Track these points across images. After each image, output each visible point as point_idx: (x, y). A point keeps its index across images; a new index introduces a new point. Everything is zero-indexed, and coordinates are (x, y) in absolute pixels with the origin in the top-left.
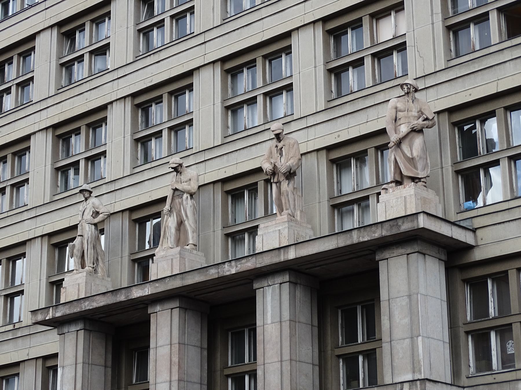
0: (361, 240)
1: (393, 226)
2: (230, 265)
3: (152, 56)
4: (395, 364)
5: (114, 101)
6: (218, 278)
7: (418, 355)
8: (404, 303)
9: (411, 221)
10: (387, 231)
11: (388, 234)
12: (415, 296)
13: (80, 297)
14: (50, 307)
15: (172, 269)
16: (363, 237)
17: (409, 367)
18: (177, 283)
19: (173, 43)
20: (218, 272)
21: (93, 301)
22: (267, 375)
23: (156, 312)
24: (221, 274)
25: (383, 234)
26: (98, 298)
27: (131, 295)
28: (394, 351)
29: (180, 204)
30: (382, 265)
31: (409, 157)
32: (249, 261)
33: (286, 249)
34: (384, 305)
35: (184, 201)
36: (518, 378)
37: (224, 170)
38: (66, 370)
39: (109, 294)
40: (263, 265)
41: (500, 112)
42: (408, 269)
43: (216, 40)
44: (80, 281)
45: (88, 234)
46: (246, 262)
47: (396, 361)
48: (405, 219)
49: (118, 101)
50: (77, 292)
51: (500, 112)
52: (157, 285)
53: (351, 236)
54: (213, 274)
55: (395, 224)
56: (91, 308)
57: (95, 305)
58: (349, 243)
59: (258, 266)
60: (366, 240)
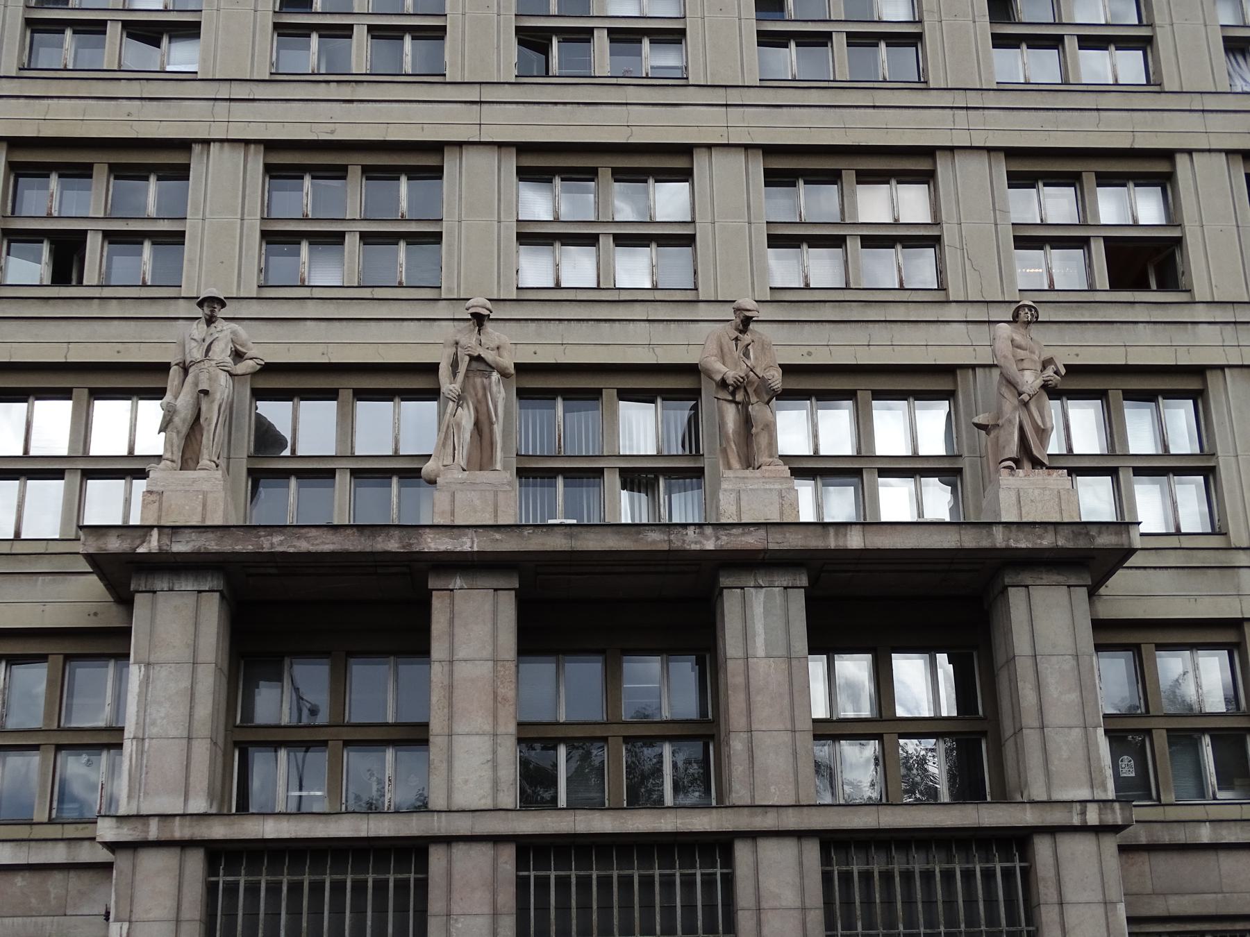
0: (1013, 544)
1: (1080, 534)
2: (702, 534)
3: (332, 85)
4: (1053, 768)
5: (215, 140)
6: (669, 551)
7: (1099, 759)
8: (1067, 667)
9: (1116, 534)
10: (1067, 539)
11: (1070, 545)
12: (1087, 658)
13: (208, 523)
14: (152, 527)
15: (496, 511)
16: (1016, 541)
17: (1084, 776)
18: (211, 544)
19: (312, 79)
20: (670, 541)
21: (299, 538)
22: (757, 753)
23: (452, 590)
24: (677, 545)
25: (1060, 543)
26: (314, 532)
27: (419, 544)
28: (1051, 747)
29: (484, 388)
30: (439, 604)
31: (1038, 427)
32: (750, 533)
33: (842, 529)
34: (1023, 667)
35: (493, 384)
36: (1245, 817)
37: (533, 348)
38: (161, 674)
39: (349, 531)
40: (785, 546)
41: (346, 395)
42: (196, 625)
43: (508, 106)
44: (206, 487)
45: (223, 393)
46: (743, 534)
47: (1056, 762)
48: (1104, 528)
49: (226, 144)
50: (200, 509)
51: (346, 395)
52: (498, 536)
53: (990, 535)
54: (654, 542)
55: (1084, 531)
56: (291, 550)
57: (303, 546)
58: (985, 543)
59: (771, 546)
60: (1023, 546)
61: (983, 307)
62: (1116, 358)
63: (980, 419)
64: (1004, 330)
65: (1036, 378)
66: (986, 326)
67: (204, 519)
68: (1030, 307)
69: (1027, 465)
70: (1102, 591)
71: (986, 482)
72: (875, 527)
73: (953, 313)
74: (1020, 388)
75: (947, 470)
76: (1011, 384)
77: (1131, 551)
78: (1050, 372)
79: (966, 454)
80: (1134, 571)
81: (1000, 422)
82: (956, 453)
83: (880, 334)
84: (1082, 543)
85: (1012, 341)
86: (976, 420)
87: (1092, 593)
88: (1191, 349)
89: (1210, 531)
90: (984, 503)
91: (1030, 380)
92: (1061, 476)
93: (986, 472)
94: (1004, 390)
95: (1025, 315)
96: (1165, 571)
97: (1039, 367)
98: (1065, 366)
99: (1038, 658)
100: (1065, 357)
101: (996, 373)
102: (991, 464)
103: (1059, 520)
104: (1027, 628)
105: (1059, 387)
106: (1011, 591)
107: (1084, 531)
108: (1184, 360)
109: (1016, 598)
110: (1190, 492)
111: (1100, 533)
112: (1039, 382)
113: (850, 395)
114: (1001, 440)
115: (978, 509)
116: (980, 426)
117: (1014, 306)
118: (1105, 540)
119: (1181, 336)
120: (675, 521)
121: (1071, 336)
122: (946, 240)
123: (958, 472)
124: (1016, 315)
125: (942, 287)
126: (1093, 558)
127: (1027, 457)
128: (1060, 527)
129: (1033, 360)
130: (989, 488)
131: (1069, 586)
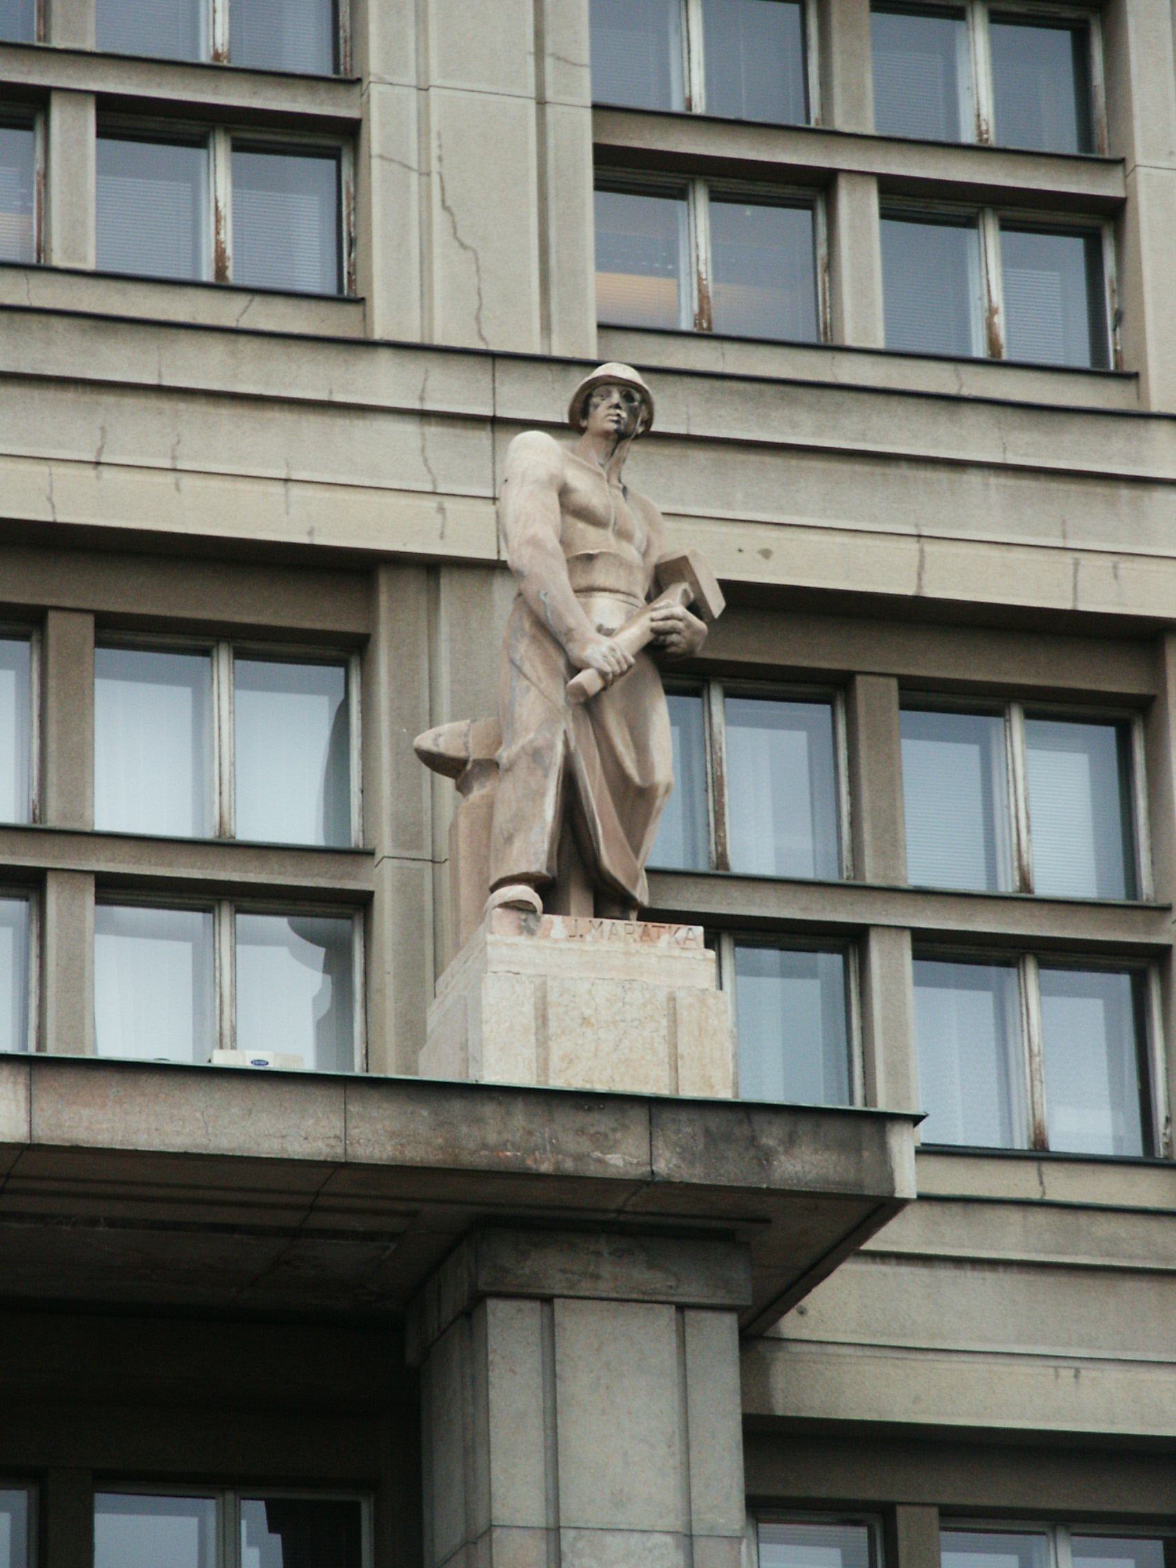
10: (686, 1154)
11: (695, 1174)
31: (625, 778)
48: (805, 1127)
61: (479, 374)
62: (885, 572)
63: (444, 737)
64: (536, 454)
65: (630, 618)
66: (482, 437)
67: (736, 1095)
68: (628, 389)
69: (578, 899)
70: (790, 1325)
71: (433, 950)
72: (69, 1078)
73: (382, 381)
74: (575, 650)
75: (326, 904)
76: (550, 634)
77: (887, 1207)
78: (673, 603)
79: (385, 845)
80: (889, 1269)
81: (504, 755)
82: (355, 839)
83: (137, 432)
84: (733, 1170)
85: (564, 492)
86: (426, 740)
87: (757, 1335)
88: (1125, 565)
89: (1135, 1149)
90: (433, 1017)
91: (612, 630)
92: (682, 945)
93: (446, 911)
94: (525, 651)
95: (604, 415)
96: (990, 1276)
97: (641, 585)
98: (727, 587)
99: (568, 1536)
100: (723, 558)
101: (502, 593)
102: (465, 890)
103: (665, 1091)
104: (534, 1434)
105: (700, 653)
106: (498, 1310)
107: (741, 1131)
108: (1101, 595)
109: (510, 1333)
110: (1072, 1022)
111: (790, 1141)
112: (633, 635)
113: (831, 688)
114: (502, 816)
115: (414, 1032)
116: (437, 762)
117: (580, 379)
118: (803, 1165)
119: (1093, 520)
120: (51, 1052)
121: (751, 488)
122: (376, 138)
123: (359, 904)
124: (582, 407)
125: (348, 296)
126: (767, 1221)
127: (580, 879)
128: (666, 1115)
129: (622, 563)
130: (453, 967)
131: (681, 1308)
